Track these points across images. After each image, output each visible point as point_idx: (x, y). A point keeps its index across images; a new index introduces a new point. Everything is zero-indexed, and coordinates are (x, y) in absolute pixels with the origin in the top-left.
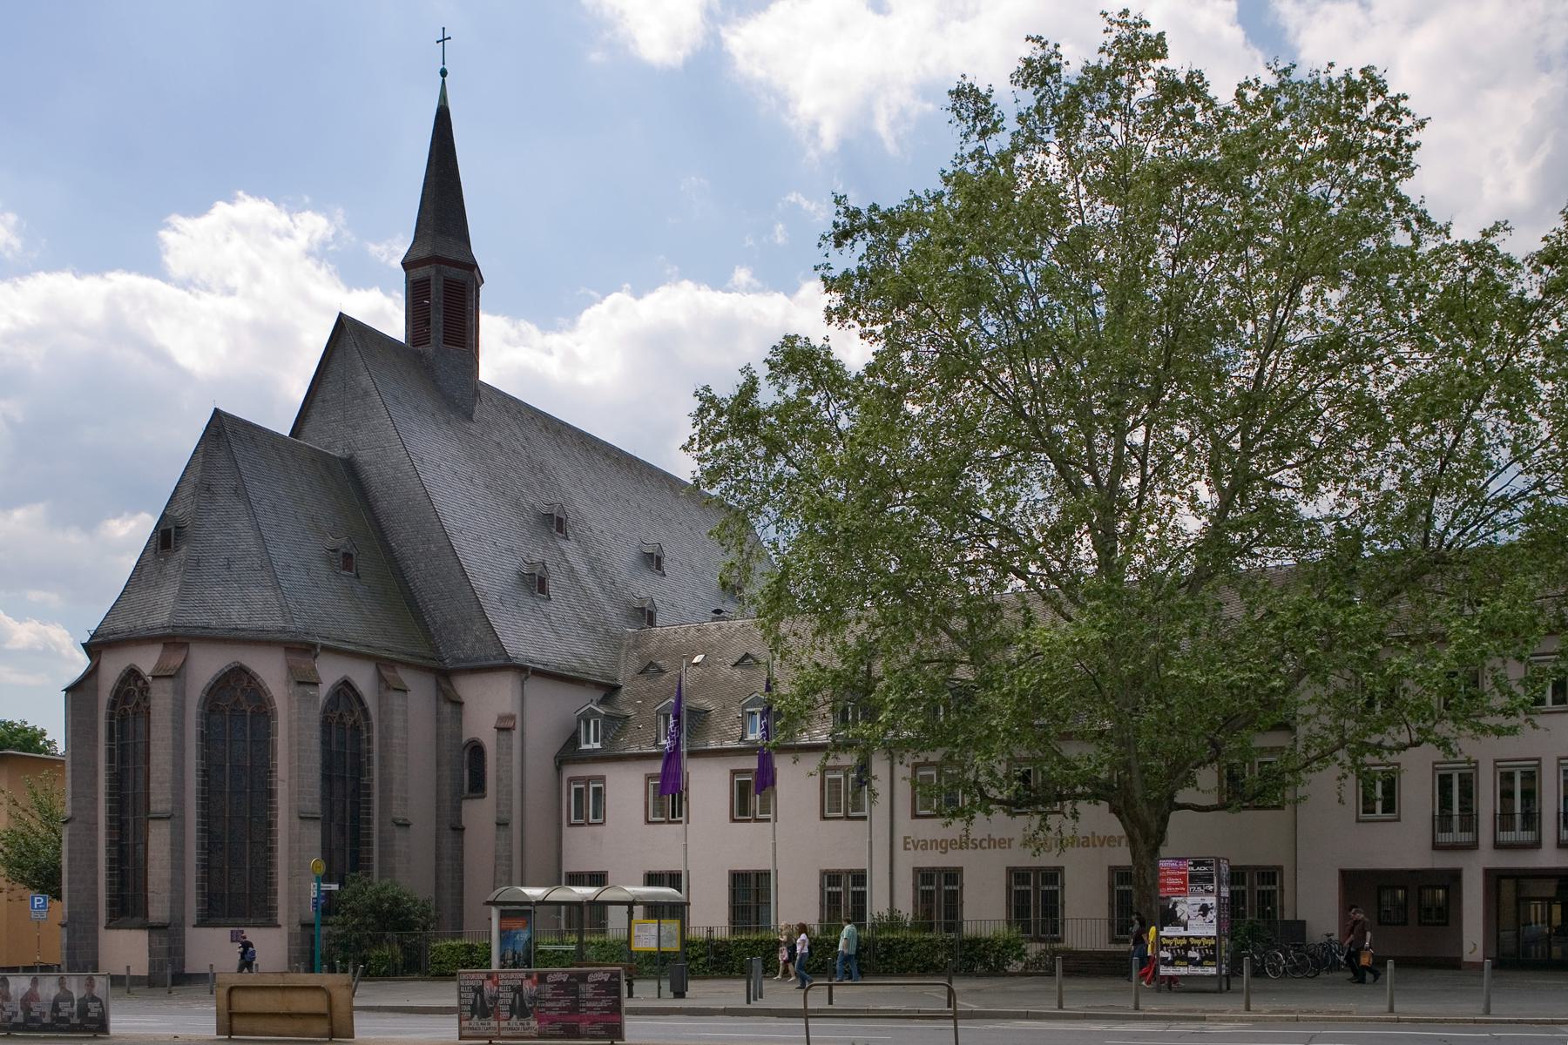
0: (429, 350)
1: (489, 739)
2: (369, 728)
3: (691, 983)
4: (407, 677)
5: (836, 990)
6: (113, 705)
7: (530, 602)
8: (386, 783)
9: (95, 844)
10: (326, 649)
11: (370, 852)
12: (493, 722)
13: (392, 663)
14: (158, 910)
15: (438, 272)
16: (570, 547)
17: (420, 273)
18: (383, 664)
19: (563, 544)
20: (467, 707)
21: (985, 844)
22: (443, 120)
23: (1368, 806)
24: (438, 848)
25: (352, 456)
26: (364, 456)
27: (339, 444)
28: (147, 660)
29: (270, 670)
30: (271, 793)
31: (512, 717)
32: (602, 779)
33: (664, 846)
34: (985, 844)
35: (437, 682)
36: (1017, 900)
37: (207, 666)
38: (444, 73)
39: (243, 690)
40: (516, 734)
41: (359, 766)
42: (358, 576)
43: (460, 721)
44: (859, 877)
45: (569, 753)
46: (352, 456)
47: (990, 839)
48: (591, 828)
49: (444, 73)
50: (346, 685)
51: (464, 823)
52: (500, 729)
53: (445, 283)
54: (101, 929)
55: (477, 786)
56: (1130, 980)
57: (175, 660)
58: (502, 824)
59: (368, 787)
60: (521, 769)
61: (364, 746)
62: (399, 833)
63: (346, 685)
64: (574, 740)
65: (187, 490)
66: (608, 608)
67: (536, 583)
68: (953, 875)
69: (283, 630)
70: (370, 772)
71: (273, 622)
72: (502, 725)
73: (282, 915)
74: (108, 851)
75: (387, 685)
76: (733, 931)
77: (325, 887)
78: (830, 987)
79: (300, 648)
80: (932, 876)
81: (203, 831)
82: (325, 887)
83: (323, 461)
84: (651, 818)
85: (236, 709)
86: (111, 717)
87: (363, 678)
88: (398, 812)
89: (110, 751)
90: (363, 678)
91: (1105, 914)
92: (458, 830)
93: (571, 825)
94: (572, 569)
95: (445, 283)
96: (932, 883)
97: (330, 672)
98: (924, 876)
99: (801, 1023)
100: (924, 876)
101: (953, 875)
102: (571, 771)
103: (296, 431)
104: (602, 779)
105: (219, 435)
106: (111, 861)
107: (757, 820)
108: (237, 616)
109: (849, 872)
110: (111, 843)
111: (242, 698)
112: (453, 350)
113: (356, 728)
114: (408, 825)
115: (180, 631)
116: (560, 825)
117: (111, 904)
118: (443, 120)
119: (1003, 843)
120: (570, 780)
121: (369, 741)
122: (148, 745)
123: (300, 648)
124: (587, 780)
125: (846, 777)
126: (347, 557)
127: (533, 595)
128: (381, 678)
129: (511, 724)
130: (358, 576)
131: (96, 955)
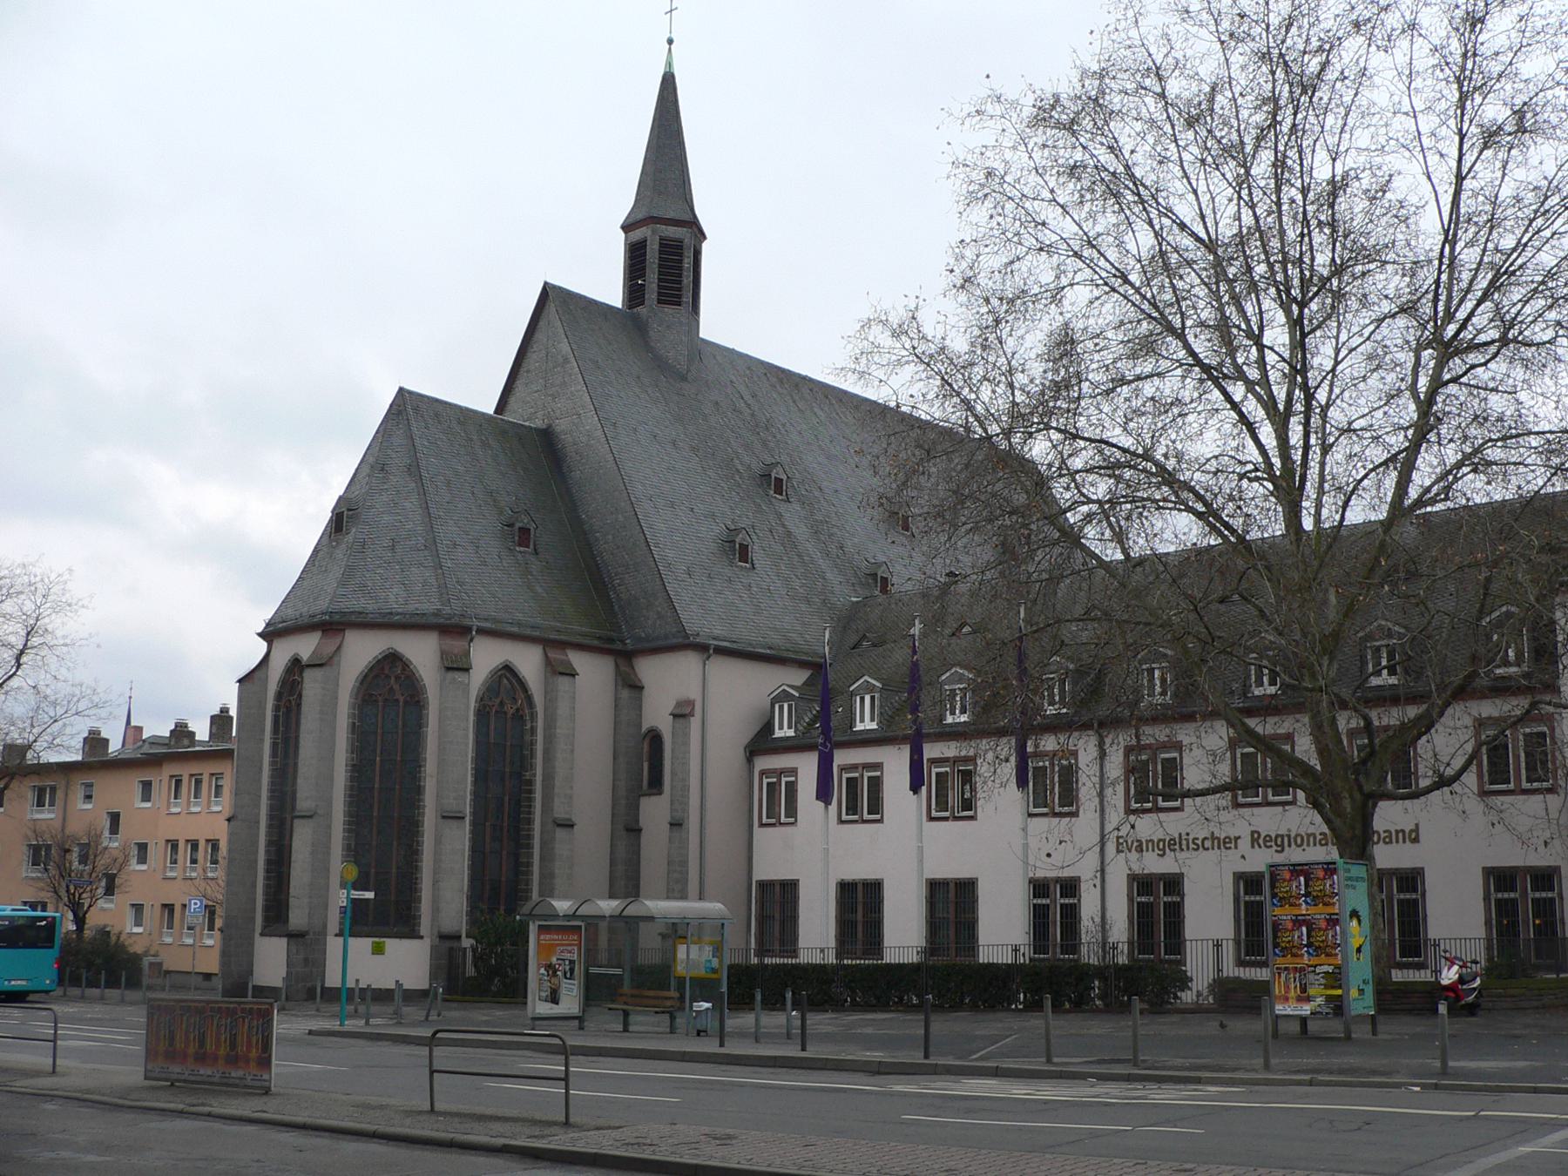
0: (642, 310)
1: (665, 725)
2: (533, 716)
3: (1353, 1013)
4: (578, 660)
5: (632, 1018)
6: (279, 696)
7: (727, 571)
8: (549, 778)
9: (255, 843)
10: (481, 631)
11: (531, 855)
12: (670, 707)
13: (563, 645)
14: (297, 918)
15: (654, 232)
16: (792, 514)
17: (638, 235)
18: (552, 644)
19: (783, 508)
20: (646, 692)
21: (1208, 844)
22: (668, 84)
23: (853, 807)
24: (612, 853)
25: (550, 426)
26: (561, 426)
27: (540, 415)
28: (305, 647)
29: (421, 652)
30: (419, 791)
31: (691, 703)
32: (878, 766)
33: (952, 850)
34: (1208, 844)
35: (617, 666)
36: (1499, 914)
37: (361, 650)
38: (670, 42)
39: (397, 678)
40: (695, 722)
41: (523, 762)
42: (536, 552)
43: (640, 708)
44: (1070, 887)
45: (762, 742)
46: (550, 426)
47: (1213, 837)
48: (783, 829)
49: (670, 42)
50: (508, 670)
51: (642, 823)
52: (675, 716)
53: (665, 250)
54: (257, 935)
55: (656, 784)
56: (783, 1009)
57: (330, 648)
58: (676, 824)
59: (530, 783)
60: (711, 759)
61: (527, 738)
62: (560, 834)
63: (508, 670)
64: (768, 727)
65: (366, 470)
66: (829, 575)
67: (738, 551)
68: (1174, 883)
69: (437, 614)
70: (532, 767)
71: (427, 605)
72: (677, 711)
73: (425, 926)
74: (267, 852)
75: (559, 671)
76: (839, 955)
77: (356, 894)
78: (626, 1014)
79: (454, 629)
80: (1513, 879)
81: (349, 831)
82: (356, 894)
83: (520, 434)
84: (844, 817)
85: (390, 694)
86: (277, 708)
87: (528, 662)
88: (560, 812)
89: (274, 745)
90: (528, 662)
91: (1481, 932)
92: (634, 830)
93: (762, 825)
94: (789, 534)
95: (665, 250)
96: (1513, 889)
97: (486, 657)
98: (1142, 884)
99: (425, 1051)
100: (1142, 884)
101: (1174, 883)
102: (763, 763)
103: (501, 407)
104: (793, 771)
105: (400, 413)
106: (268, 862)
107: (1056, 815)
108: (395, 599)
109: (1057, 880)
110: (269, 843)
111: (396, 687)
112: (668, 309)
113: (519, 717)
114: (572, 826)
115: (337, 617)
116: (751, 827)
117: (267, 909)
118: (668, 84)
119: (1228, 843)
120: (763, 773)
121: (533, 730)
122: (297, 738)
123: (454, 629)
124: (781, 772)
125: (1052, 765)
126: (524, 532)
127: (731, 564)
128: (548, 662)
129: (687, 711)
130: (536, 552)
131: (251, 964)
